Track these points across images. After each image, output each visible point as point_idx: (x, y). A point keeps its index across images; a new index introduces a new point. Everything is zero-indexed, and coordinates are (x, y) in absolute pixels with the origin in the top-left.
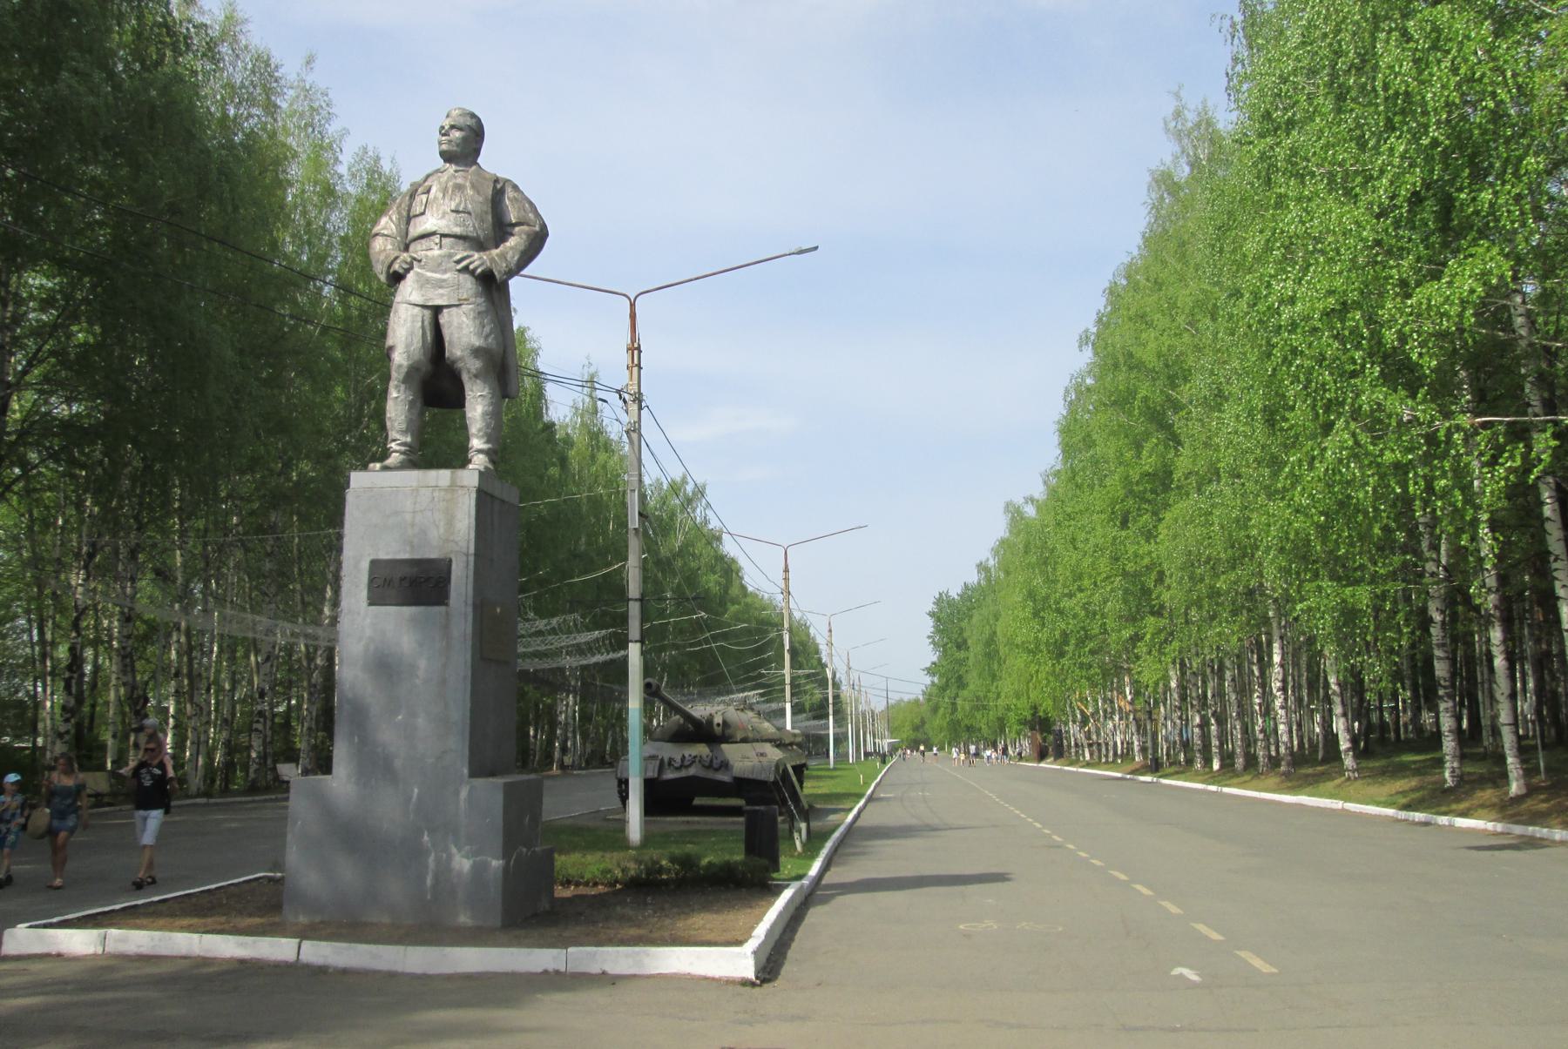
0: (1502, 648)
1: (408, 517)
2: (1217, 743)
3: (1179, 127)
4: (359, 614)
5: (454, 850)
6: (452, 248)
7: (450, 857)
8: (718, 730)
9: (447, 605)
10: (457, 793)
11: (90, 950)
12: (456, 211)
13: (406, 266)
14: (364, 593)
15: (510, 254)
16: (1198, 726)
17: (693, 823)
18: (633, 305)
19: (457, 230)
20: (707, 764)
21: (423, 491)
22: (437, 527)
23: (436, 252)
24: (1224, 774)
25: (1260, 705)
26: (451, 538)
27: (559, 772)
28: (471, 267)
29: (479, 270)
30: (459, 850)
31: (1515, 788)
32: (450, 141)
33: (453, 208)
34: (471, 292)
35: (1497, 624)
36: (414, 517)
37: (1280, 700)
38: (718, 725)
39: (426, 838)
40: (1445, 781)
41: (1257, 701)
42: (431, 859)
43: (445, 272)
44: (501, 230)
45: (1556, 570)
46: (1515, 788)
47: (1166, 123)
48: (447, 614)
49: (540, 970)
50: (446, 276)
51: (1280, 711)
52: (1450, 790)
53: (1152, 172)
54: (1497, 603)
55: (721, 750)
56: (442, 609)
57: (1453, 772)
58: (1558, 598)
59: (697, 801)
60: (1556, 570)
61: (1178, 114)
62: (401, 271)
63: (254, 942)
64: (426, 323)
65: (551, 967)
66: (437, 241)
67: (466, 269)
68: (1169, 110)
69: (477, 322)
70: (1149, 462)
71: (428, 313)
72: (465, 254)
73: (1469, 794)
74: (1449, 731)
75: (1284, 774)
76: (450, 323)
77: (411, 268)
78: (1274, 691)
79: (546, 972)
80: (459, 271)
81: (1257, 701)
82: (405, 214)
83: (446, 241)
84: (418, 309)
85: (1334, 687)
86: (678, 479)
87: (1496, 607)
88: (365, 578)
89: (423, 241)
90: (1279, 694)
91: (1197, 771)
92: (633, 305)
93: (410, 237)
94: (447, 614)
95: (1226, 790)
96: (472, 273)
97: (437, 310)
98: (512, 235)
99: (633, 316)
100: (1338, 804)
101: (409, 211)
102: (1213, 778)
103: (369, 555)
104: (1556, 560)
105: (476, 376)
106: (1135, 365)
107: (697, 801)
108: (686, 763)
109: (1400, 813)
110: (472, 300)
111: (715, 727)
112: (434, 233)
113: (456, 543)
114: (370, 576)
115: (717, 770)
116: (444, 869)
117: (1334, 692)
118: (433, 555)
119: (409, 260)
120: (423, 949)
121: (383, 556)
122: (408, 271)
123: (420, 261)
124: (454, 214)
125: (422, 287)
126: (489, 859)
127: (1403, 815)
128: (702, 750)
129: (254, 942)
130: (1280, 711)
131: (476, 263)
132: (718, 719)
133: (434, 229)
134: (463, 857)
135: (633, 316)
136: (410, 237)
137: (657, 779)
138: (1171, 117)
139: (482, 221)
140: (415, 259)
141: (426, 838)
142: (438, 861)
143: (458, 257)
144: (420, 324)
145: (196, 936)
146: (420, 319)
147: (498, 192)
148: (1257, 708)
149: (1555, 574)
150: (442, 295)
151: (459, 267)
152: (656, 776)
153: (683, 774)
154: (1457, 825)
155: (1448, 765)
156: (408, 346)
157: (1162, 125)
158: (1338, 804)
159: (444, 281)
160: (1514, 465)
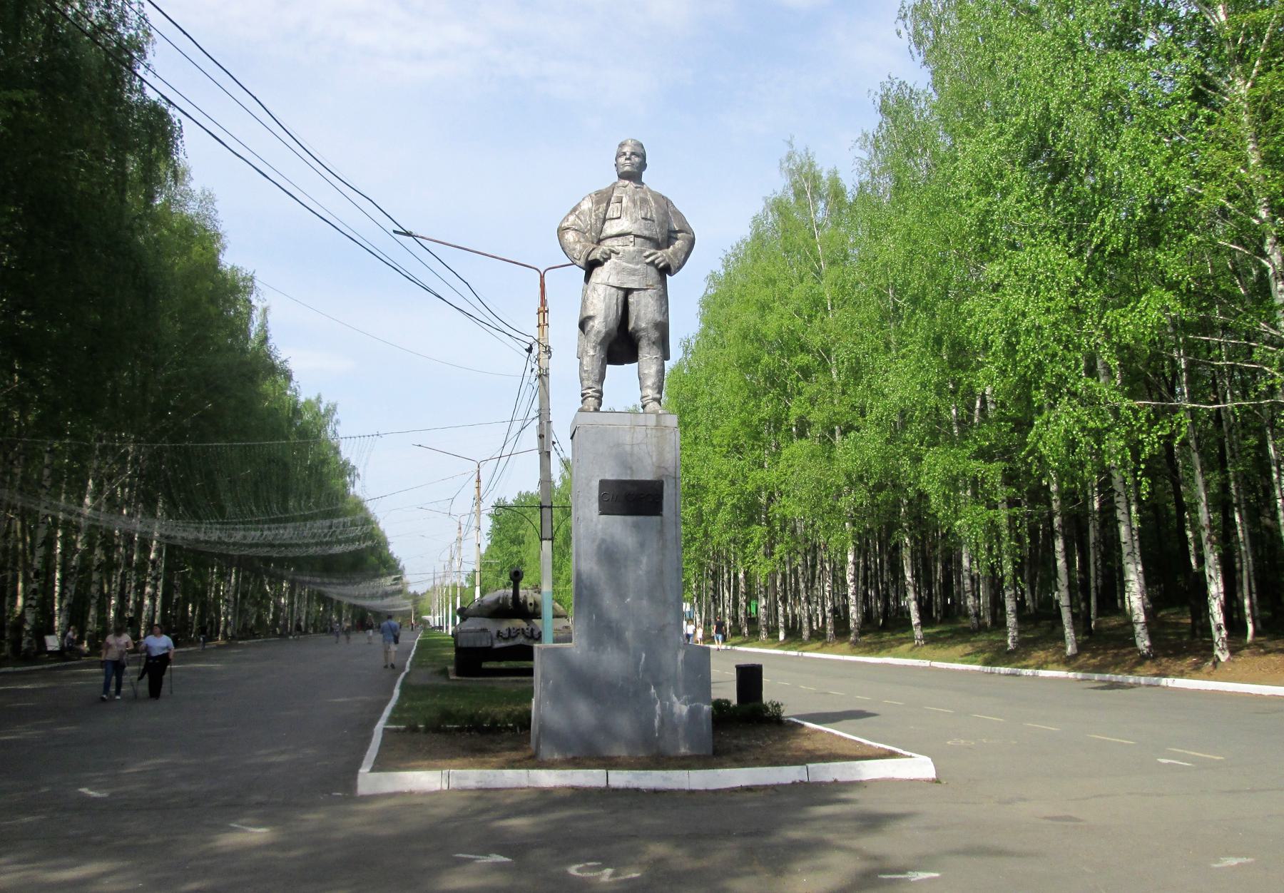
0: (1063, 554)
1: (628, 448)
2: (783, 620)
3: (791, 167)
4: (592, 521)
5: (675, 699)
6: (642, 246)
7: (672, 705)
8: (530, 608)
9: (661, 515)
10: (676, 655)
11: (437, 786)
12: (645, 219)
13: (605, 257)
14: (596, 505)
15: (679, 254)
16: (765, 607)
17: (525, 681)
18: (542, 277)
19: (646, 233)
20: (507, 636)
21: (638, 429)
22: (651, 456)
23: (631, 248)
24: (789, 643)
25: (829, 591)
26: (663, 465)
27: (224, 642)
28: (656, 262)
29: (662, 265)
30: (678, 697)
31: (1070, 649)
32: (633, 164)
33: (643, 216)
34: (655, 280)
35: (1060, 537)
36: (632, 448)
37: (852, 589)
38: (531, 604)
39: (653, 690)
40: (1007, 646)
41: (828, 589)
42: (658, 707)
43: (637, 264)
44: (670, 238)
45: (1118, 502)
46: (1070, 649)
47: (781, 164)
48: (662, 522)
49: (790, 782)
50: (639, 267)
51: (852, 597)
52: (1012, 652)
53: (765, 199)
54: (1060, 523)
55: (535, 624)
56: (657, 518)
57: (1014, 639)
58: (1119, 521)
59: (486, 665)
60: (1118, 502)
61: (789, 158)
62: (602, 260)
63: (572, 774)
64: (620, 300)
65: (797, 778)
66: (632, 239)
67: (652, 263)
68: (784, 155)
69: (659, 303)
70: (767, 410)
71: (621, 293)
72: (652, 251)
73: (1027, 655)
74: (1012, 611)
75: (853, 642)
76: (638, 303)
77: (610, 258)
78: (848, 582)
79: (794, 783)
80: (648, 264)
81: (828, 589)
82: (602, 216)
83: (639, 240)
84: (615, 289)
85: (909, 579)
86: (313, 398)
87: (1059, 526)
88: (595, 493)
89: (620, 239)
90: (851, 584)
91: (762, 641)
92: (542, 277)
93: (604, 235)
94: (662, 522)
95: (806, 654)
96: (656, 266)
97: (628, 292)
98: (677, 239)
99: (543, 286)
100: (927, 663)
101: (605, 214)
102: (781, 646)
103: (598, 476)
104: (1118, 496)
105: (654, 343)
106: (760, 339)
107: (486, 665)
108: (513, 634)
109: (986, 668)
110: (656, 286)
111: (529, 606)
112: (629, 234)
113: (666, 469)
114: (600, 492)
115: (514, 637)
116: (668, 713)
117: (909, 583)
118: (649, 477)
119: (608, 252)
120: (702, 771)
121: (609, 477)
122: (606, 260)
123: (618, 254)
124: (644, 221)
125: (618, 273)
126: (702, 705)
127: (988, 669)
128: (519, 623)
129: (572, 774)
130: (852, 597)
131: (660, 259)
132: (530, 600)
133: (630, 231)
134: (681, 704)
135: (543, 286)
136: (604, 235)
137: (490, 647)
138: (785, 159)
139: (662, 227)
140: (613, 252)
141: (653, 690)
142: (663, 708)
143: (647, 253)
144: (615, 301)
145: (523, 771)
146: (615, 297)
147: (665, 204)
148: (827, 594)
149: (1117, 505)
150: (635, 281)
151: (649, 260)
152: (489, 645)
153: (510, 643)
154: (1040, 675)
155: (1010, 634)
156: (606, 317)
157: (778, 164)
158: (927, 663)
159: (636, 270)
160: (1164, 433)
